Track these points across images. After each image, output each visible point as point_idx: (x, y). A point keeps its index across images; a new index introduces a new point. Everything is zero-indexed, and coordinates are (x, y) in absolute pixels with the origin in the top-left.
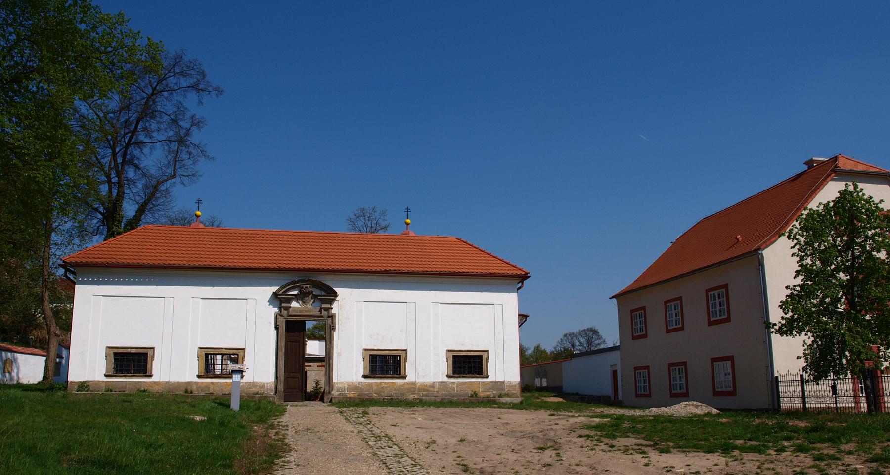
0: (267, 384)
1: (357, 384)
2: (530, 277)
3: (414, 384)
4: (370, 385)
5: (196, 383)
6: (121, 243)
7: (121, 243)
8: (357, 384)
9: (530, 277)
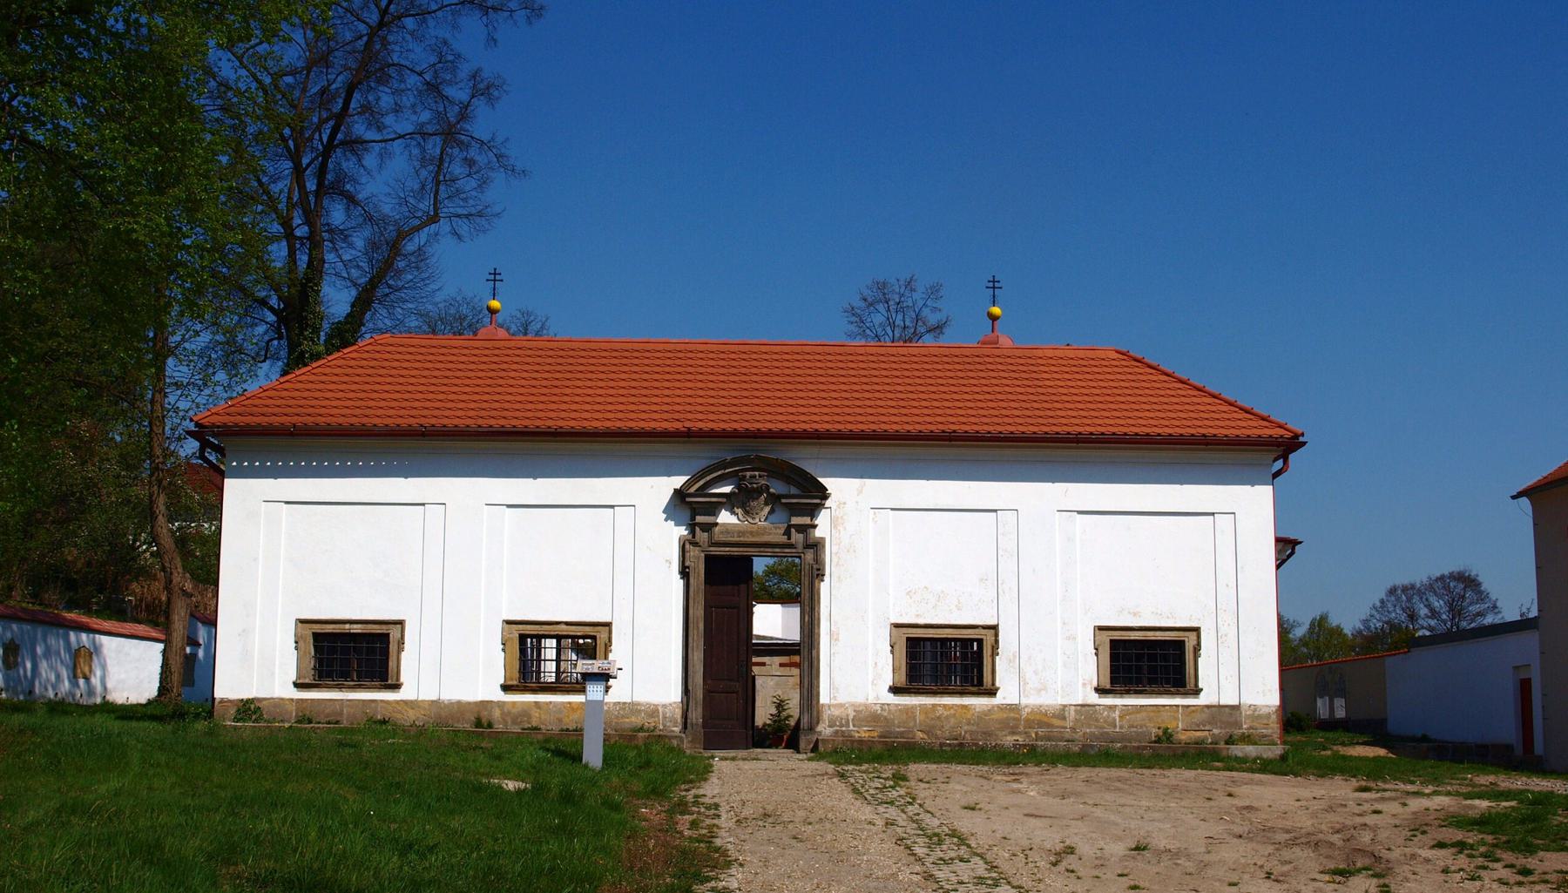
0: (664, 706)
1: (878, 708)
2: (1305, 443)
3: (1014, 708)
4: (908, 710)
5: (501, 704)
6: (323, 378)
7: (323, 378)
8: (878, 708)
9: (1305, 443)
